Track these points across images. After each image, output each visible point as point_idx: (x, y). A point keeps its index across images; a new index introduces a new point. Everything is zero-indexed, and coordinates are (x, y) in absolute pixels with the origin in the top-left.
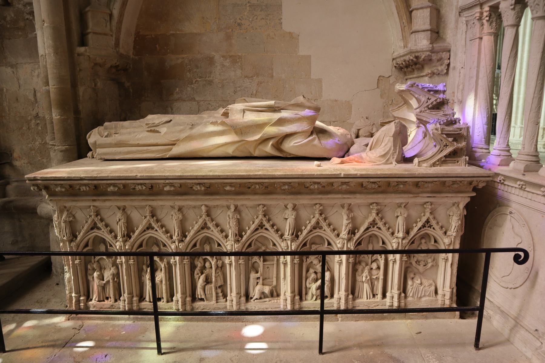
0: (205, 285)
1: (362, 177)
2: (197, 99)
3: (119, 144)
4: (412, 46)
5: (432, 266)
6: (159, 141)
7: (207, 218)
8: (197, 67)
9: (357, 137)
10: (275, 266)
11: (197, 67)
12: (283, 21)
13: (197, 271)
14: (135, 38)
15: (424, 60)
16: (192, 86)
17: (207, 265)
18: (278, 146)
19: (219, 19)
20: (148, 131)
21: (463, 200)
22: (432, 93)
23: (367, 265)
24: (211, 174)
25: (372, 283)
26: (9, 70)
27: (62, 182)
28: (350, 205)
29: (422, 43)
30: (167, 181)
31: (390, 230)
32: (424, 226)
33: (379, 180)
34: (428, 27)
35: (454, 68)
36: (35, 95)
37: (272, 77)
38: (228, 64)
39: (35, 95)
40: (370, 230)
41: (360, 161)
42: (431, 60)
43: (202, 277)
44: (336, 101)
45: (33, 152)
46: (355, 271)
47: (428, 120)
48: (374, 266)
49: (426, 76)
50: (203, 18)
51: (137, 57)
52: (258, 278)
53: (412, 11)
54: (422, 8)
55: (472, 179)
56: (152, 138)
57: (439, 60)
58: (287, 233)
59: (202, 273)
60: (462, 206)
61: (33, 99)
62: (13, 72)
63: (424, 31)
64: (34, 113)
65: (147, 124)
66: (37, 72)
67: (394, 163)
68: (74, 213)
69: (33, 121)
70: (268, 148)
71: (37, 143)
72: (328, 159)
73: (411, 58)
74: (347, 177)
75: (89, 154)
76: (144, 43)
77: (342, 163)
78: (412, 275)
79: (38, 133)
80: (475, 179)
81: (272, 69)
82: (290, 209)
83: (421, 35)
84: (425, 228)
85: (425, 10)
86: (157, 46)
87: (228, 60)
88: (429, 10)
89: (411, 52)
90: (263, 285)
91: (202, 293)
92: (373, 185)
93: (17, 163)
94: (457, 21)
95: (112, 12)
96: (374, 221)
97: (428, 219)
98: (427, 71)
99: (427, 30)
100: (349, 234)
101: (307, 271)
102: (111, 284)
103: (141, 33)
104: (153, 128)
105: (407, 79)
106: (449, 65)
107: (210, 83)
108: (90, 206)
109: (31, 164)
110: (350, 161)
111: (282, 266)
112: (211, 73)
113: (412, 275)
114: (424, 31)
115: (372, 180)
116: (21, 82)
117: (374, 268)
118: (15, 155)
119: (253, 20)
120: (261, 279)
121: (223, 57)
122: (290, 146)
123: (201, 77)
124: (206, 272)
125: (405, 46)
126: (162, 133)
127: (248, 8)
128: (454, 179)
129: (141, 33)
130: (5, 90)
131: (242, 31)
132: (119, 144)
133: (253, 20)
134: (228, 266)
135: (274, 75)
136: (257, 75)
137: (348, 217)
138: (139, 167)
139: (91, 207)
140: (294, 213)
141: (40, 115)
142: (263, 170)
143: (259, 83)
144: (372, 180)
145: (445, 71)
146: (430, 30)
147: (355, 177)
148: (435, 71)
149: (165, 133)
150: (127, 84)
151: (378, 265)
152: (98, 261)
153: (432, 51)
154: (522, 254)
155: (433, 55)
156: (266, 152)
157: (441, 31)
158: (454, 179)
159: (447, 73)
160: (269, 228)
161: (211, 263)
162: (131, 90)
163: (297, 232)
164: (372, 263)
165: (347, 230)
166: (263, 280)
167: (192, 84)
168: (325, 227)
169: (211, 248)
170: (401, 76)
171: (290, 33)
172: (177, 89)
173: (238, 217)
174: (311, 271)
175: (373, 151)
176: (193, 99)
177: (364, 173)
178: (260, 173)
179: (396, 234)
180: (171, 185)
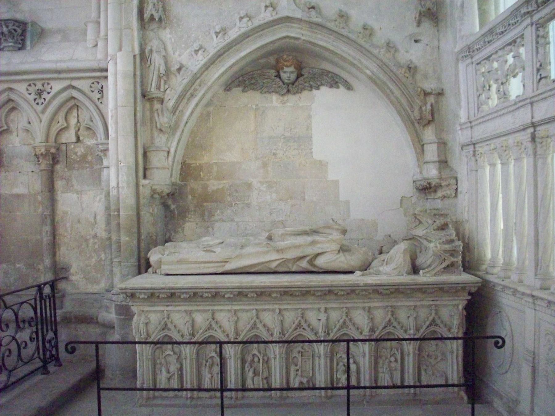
0: (254, 376)
1: (376, 285)
2: (236, 220)
3: (180, 262)
4: (425, 175)
5: (442, 359)
6: (214, 260)
7: (257, 321)
8: (237, 191)
9: (381, 253)
10: (311, 359)
11: (237, 191)
12: (313, 150)
13: (247, 365)
14: (182, 166)
15: (435, 186)
16: (232, 208)
17: (256, 359)
18: (311, 262)
19: (257, 149)
20: (204, 251)
21: (461, 302)
22: (437, 216)
23: (387, 358)
24: (262, 284)
25: (391, 374)
26: (75, 196)
27: (145, 291)
28: (370, 308)
29: (432, 172)
30: (229, 290)
31: (404, 328)
32: (431, 325)
33: (391, 287)
34: (436, 159)
35: (461, 193)
36: (95, 218)
37: (304, 199)
38: (264, 189)
39: (95, 218)
40: (387, 328)
41: (378, 273)
42: (441, 186)
43: (252, 370)
44: (363, 220)
45: (89, 268)
46: (376, 363)
47: (431, 239)
48: (393, 359)
49: (438, 198)
50: (242, 149)
51: (182, 183)
52: (297, 370)
53: (423, 145)
54: (431, 143)
55: (465, 285)
56: (208, 257)
57: (448, 185)
58: (320, 332)
59: (251, 367)
60: (460, 307)
61: (93, 221)
62: (78, 198)
63: (433, 162)
64: (93, 233)
65: (203, 245)
66: (98, 197)
67: (405, 274)
68: (149, 316)
69: (92, 240)
70: (304, 264)
71: (93, 260)
72: (352, 272)
73: (425, 184)
74: (366, 285)
75: (150, 270)
76: (187, 171)
77: (363, 275)
78: (424, 367)
79: (95, 251)
80: (467, 285)
81: (304, 193)
82: (323, 312)
83: (431, 166)
84: (432, 327)
85: (433, 145)
86: (201, 173)
87: (264, 186)
88: (436, 145)
89: (425, 179)
90: (302, 376)
91: (251, 382)
92: (387, 292)
93: (73, 278)
94: (460, 153)
95: (169, 149)
96: (389, 321)
97: (434, 319)
98: (440, 194)
99: (436, 162)
100: (370, 331)
101: (337, 364)
102: (176, 376)
103: (187, 162)
104: (208, 249)
105: (427, 199)
106: (457, 189)
107: (248, 205)
108: (163, 311)
109: (86, 279)
110: (370, 274)
111: (317, 359)
112: (249, 196)
113: (424, 367)
114: (433, 162)
115: (385, 288)
116: (84, 206)
117: (393, 361)
118: (72, 270)
119: (286, 150)
120: (300, 371)
121: (261, 182)
122: (321, 262)
123: (240, 201)
124: (255, 365)
125: (421, 173)
126: (217, 253)
127: (282, 140)
128: (450, 285)
129: (187, 162)
130: (69, 213)
131: (277, 160)
132: (180, 262)
133: (286, 150)
134: (273, 360)
135: (306, 197)
136: (291, 198)
137: (369, 317)
138: (512, 241)
139: (165, 312)
140: (326, 315)
141: (98, 235)
142: (301, 281)
143: (293, 206)
144: (385, 288)
145: (454, 195)
146: (439, 162)
147: (371, 285)
148: (446, 195)
149: (219, 253)
150: (173, 207)
151: (395, 358)
152: (165, 357)
153: (441, 179)
154: (500, 341)
155: (442, 182)
156: (303, 268)
157: (449, 160)
158: (450, 285)
159: (456, 196)
160: (307, 328)
161: (259, 358)
162: (176, 212)
163: (328, 331)
164: (391, 356)
165: (369, 328)
166: (301, 372)
167: (232, 206)
168: (351, 327)
169: (489, 107)
170: (423, 196)
171: (320, 161)
172: (218, 211)
173: (282, 319)
174: (341, 364)
175: (388, 266)
176: (232, 220)
177: (379, 282)
178: (299, 283)
179: (408, 332)
180: (231, 293)
